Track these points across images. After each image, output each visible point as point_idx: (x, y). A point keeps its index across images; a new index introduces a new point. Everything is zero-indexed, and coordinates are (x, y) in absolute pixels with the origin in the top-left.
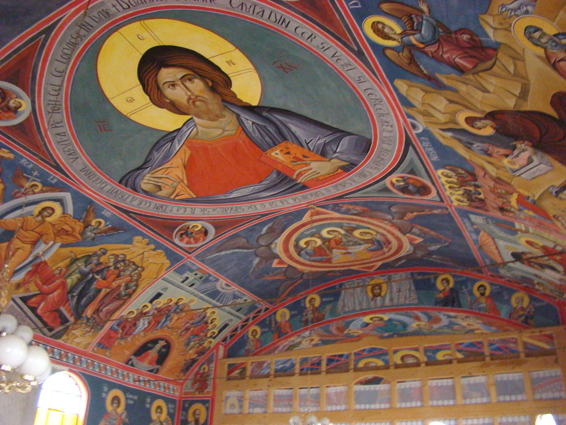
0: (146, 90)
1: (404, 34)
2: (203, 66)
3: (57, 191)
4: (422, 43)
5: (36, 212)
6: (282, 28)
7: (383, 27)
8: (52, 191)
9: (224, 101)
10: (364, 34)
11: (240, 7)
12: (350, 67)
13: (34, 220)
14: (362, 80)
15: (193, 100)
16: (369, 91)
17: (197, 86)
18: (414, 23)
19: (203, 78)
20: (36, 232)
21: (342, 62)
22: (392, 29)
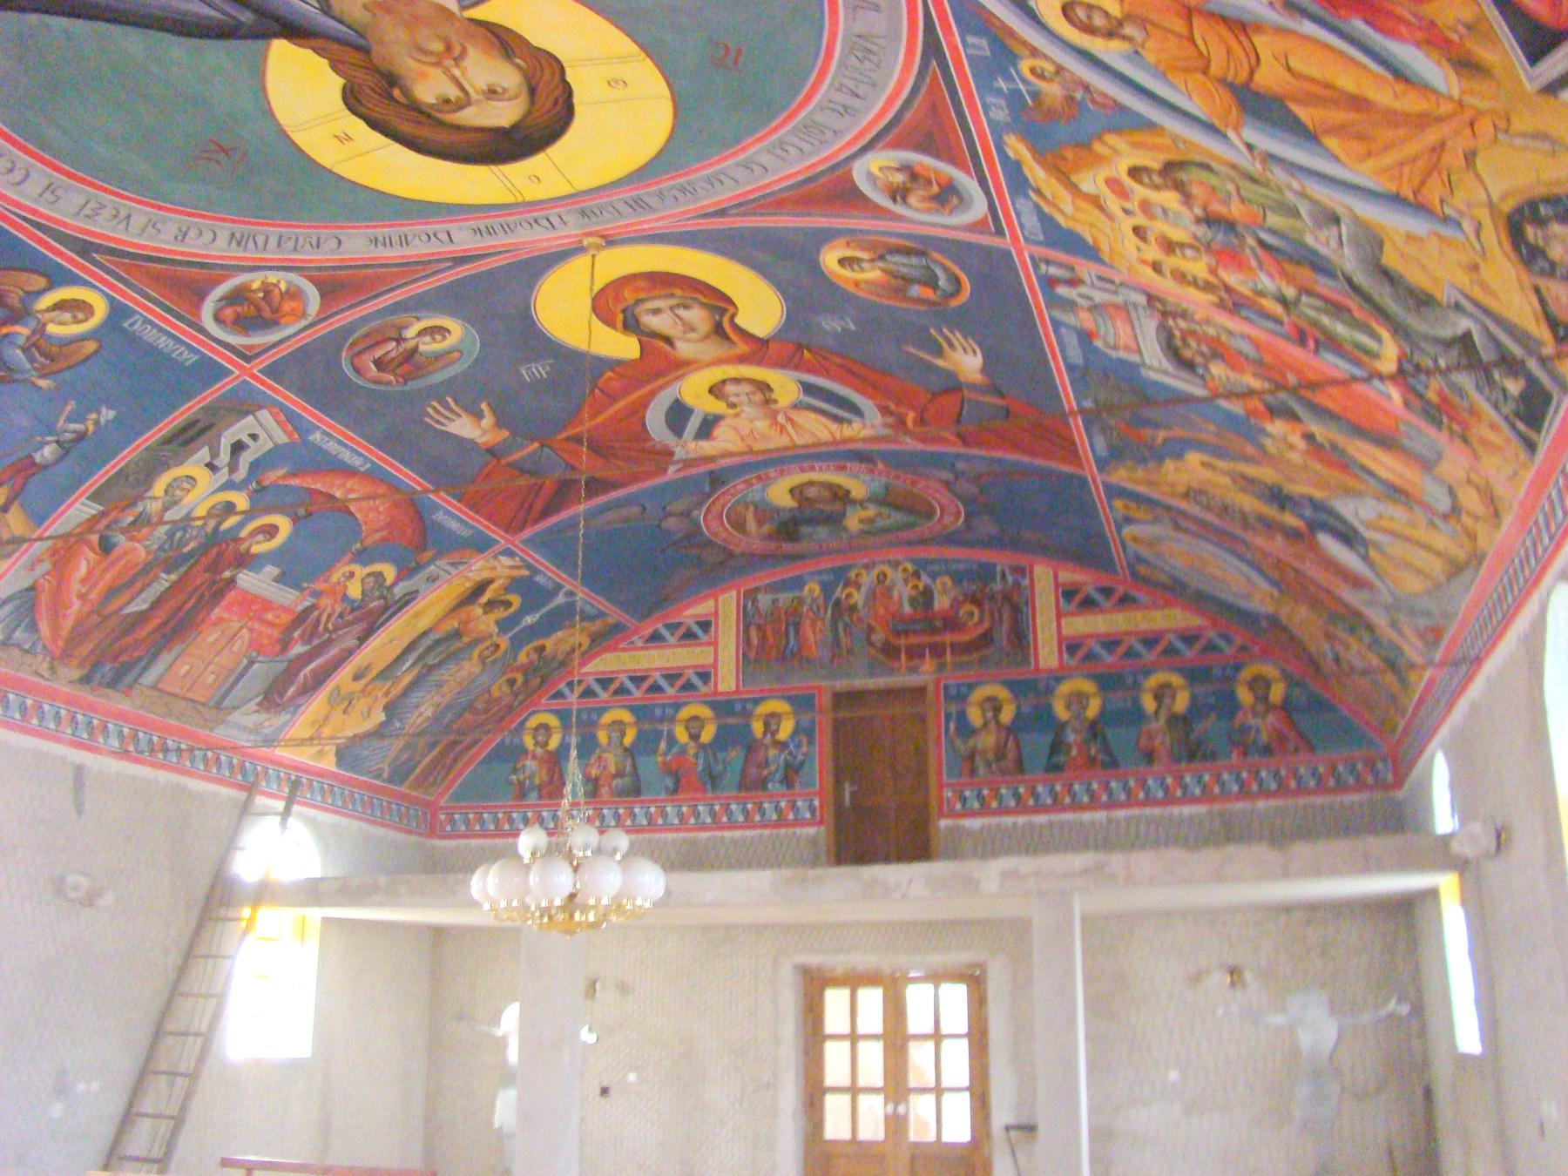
0: (568, 91)
1: (40, 330)
2: (406, 128)
3: (998, 23)
4: (7, 335)
5: (1115, 45)
6: (239, 229)
7: (75, 317)
8: (1011, 33)
9: (366, 51)
10: (100, 290)
11: (322, 240)
12: (87, 211)
13: (1149, 45)
14: (48, 195)
15: (451, 54)
16: (18, 175)
17: (430, 88)
18: (41, 354)
19: (415, 107)
20: (1191, 26)
21: (107, 213)
22: (61, 323)
